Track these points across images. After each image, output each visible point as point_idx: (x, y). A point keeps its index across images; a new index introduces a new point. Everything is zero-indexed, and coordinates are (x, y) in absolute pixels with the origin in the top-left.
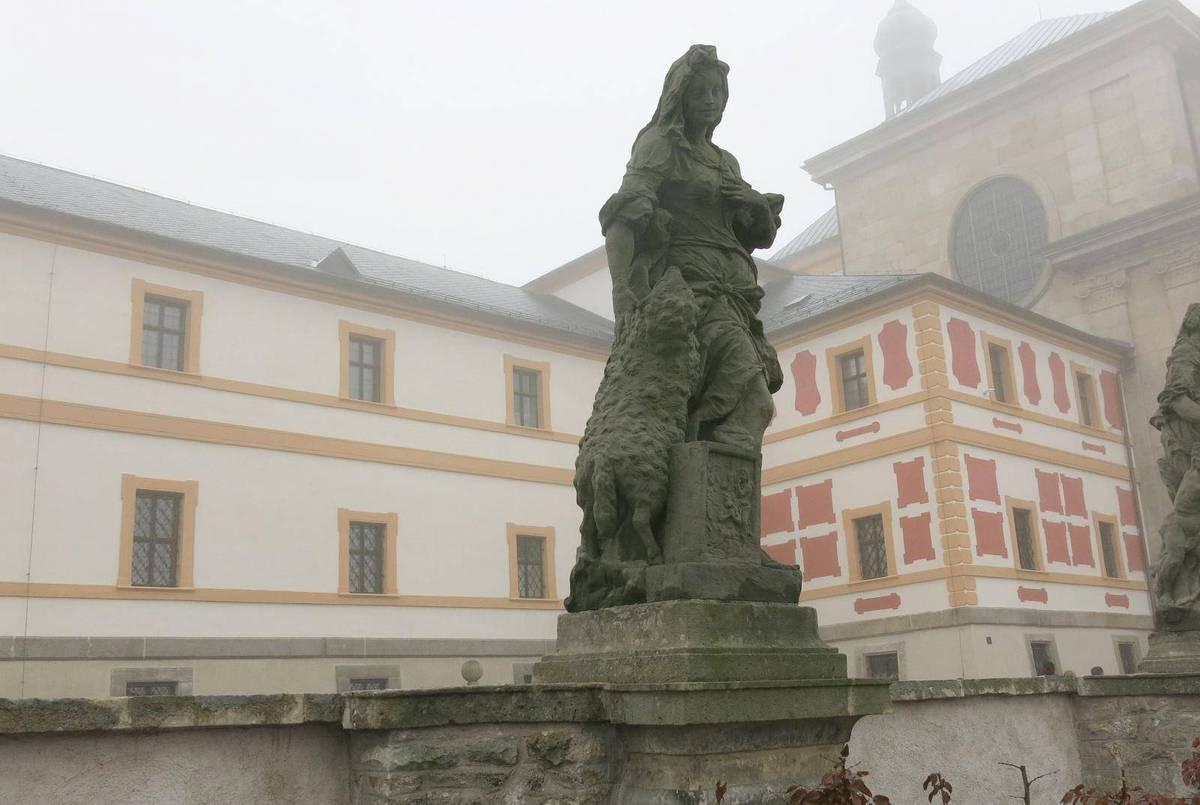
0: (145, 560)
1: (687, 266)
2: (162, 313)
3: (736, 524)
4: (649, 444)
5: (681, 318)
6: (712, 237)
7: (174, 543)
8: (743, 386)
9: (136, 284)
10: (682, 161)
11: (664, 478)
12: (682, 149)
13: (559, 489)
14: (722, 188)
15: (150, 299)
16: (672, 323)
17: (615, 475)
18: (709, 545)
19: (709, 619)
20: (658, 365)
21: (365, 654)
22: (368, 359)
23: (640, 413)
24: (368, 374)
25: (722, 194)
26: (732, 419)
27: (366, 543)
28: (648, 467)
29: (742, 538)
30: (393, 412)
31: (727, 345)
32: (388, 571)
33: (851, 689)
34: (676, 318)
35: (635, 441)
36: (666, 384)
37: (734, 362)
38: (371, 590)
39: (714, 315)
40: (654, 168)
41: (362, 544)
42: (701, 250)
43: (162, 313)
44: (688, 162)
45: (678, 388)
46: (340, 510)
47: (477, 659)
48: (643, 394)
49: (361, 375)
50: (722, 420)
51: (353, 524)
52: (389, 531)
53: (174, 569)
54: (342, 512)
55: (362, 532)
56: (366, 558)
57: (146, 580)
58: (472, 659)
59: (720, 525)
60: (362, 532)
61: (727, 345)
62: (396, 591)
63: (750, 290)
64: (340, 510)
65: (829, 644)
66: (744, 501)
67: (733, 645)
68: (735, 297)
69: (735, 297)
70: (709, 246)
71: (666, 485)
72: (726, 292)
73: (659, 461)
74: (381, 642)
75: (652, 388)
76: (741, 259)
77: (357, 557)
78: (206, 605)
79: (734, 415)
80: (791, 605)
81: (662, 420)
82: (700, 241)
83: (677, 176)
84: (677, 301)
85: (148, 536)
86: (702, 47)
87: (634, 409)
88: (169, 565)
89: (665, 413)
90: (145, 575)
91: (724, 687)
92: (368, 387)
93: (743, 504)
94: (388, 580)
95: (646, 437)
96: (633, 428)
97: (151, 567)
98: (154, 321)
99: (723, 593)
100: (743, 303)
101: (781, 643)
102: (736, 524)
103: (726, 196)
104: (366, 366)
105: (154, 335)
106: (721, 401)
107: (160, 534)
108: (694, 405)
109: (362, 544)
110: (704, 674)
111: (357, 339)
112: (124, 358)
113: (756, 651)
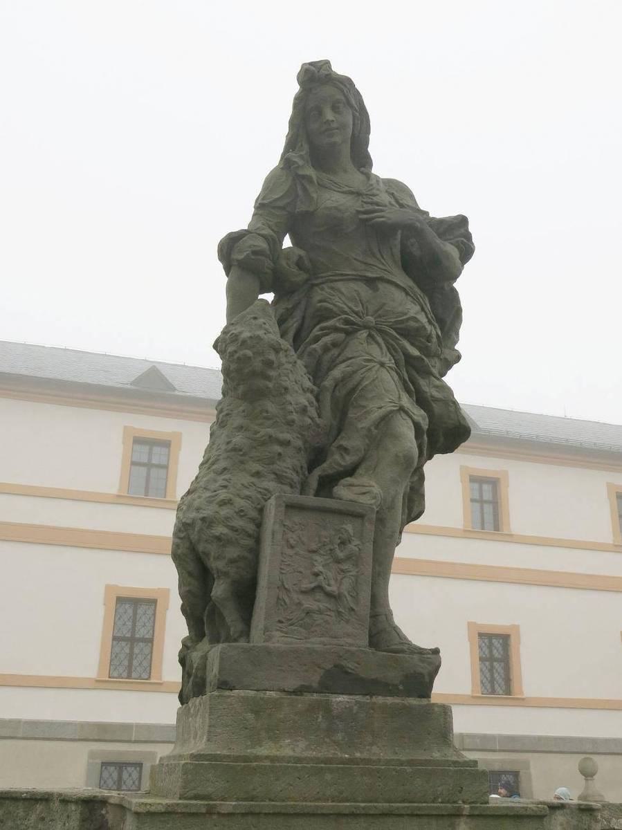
0: (488, 675)
1: (319, 305)
2: (150, 453)
3: (329, 595)
4: (223, 503)
5: (249, 353)
6: (355, 270)
7: (506, 661)
8: (369, 430)
9: (126, 429)
10: (305, 190)
11: (249, 542)
12: (304, 177)
13: (154, 558)
14: (358, 212)
15: (138, 441)
16: (239, 358)
17: (191, 543)
18: (280, 622)
19: (250, 716)
20: (244, 411)
21: (498, 748)
22: (487, 496)
23: (225, 469)
24: (488, 509)
25: (360, 219)
26: (360, 471)
27: (495, 651)
28: (220, 530)
29: (339, 613)
30: (511, 538)
31: (359, 384)
32: (514, 675)
33: (463, 820)
34: (241, 353)
35: (210, 501)
36: (256, 433)
37: (364, 403)
38: (501, 692)
39: (348, 353)
40: (271, 203)
41: (491, 652)
42: (339, 285)
43: (150, 453)
44: (311, 189)
45: (270, 437)
46: (469, 624)
47: (591, 756)
48: (230, 446)
49: (482, 509)
50: (351, 471)
51: (481, 635)
52: (513, 641)
53: (508, 680)
54: (471, 625)
55: (490, 642)
56: (495, 664)
57: (490, 690)
58: (588, 756)
59: (301, 597)
60: (490, 642)
61: (359, 384)
62: (522, 693)
63: (402, 322)
64: (469, 624)
65: (465, 753)
66: (345, 566)
67: (287, 752)
68: (380, 331)
69: (380, 331)
70: (349, 280)
71: (251, 550)
72: (365, 327)
73: (239, 523)
74: (512, 739)
75: (238, 439)
76: (393, 289)
77: (487, 663)
78: (608, 711)
79: (363, 466)
80: (413, 701)
81: (253, 476)
82: (342, 275)
83: (301, 207)
84: (241, 333)
85: (488, 656)
86: (311, 64)
87: (222, 464)
88: (489, 679)
89: (256, 467)
90: (489, 686)
91: (203, 810)
92: (489, 518)
93: (342, 571)
94: (515, 685)
95: (223, 495)
96: (213, 487)
97: (492, 681)
98: (477, 496)
99: (292, 683)
100: (395, 339)
101: (380, 752)
102: (329, 595)
103: (367, 220)
104: (486, 502)
105: (143, 471)
106: (346, 450)
107: (496, 654)
108: (317, 456)
109: (491, 652)
110: (210, 790)
111: (477, 480)
112: (114, 491)
113: (318, 760)
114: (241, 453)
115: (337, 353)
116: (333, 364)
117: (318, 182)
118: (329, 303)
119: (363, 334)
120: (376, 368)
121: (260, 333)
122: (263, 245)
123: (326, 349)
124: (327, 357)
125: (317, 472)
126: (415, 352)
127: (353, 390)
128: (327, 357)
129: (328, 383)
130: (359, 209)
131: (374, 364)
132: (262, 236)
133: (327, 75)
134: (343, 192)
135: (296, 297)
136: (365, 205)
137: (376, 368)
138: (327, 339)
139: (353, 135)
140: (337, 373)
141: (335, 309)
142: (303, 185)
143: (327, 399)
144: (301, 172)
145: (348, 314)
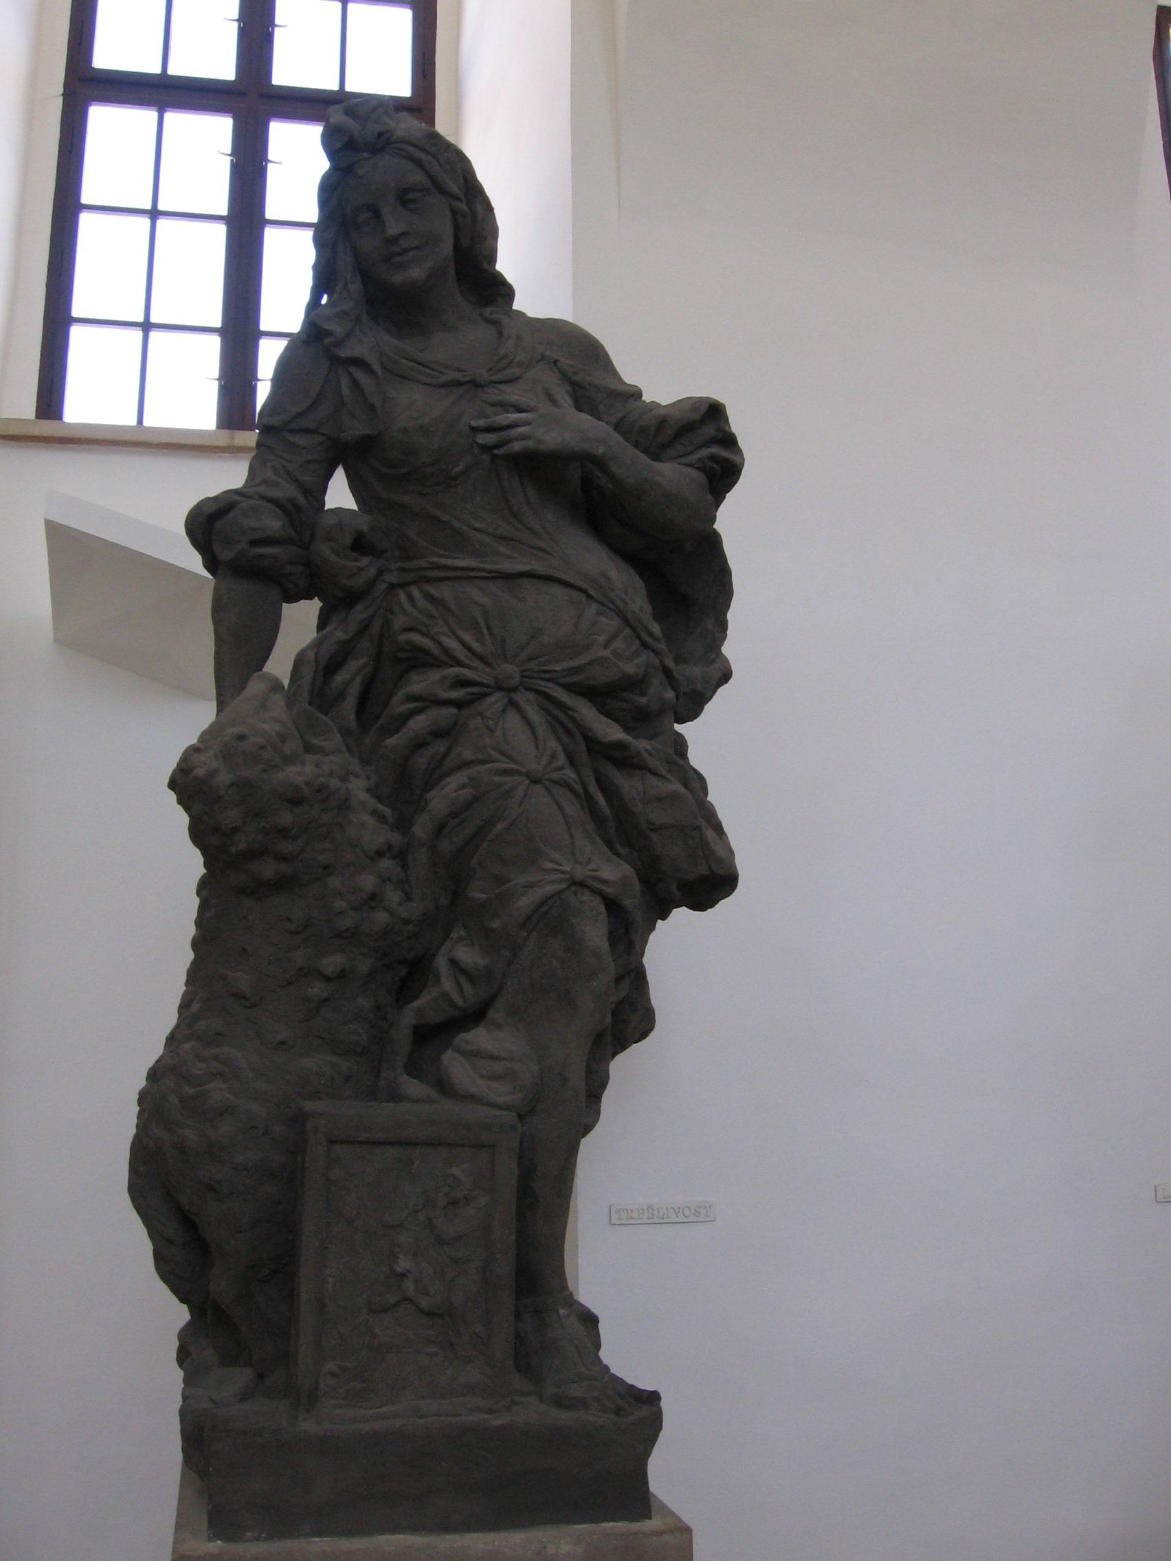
114: (247, 1004)
115: (442, 749)
116: (435, 777)
117: (383, 367)
118: (424, 634)
119: (495, 701)
120: (522, 789)
121: (252, 772)
122: (274, 524)
123: (419, 745)
124: (422, 760)
125: (407, 1018)
126: (612, 732)
127: (480, 834)
128: (422, 760)
129: (421, 828)
130: (474, 423)
131: (517, 778)
132: (274, 502)
133: (380, 135)
134: (443, 386)
135: (360, 613)
136: (489, 410)
137: (522, 789)
138: (419, 723)
139: (457, 246)
140: (440, 800)
141: (435, 650)
142: (350, 374)
143: (420, 858)
144: (345, 352)
145: (460, 664)
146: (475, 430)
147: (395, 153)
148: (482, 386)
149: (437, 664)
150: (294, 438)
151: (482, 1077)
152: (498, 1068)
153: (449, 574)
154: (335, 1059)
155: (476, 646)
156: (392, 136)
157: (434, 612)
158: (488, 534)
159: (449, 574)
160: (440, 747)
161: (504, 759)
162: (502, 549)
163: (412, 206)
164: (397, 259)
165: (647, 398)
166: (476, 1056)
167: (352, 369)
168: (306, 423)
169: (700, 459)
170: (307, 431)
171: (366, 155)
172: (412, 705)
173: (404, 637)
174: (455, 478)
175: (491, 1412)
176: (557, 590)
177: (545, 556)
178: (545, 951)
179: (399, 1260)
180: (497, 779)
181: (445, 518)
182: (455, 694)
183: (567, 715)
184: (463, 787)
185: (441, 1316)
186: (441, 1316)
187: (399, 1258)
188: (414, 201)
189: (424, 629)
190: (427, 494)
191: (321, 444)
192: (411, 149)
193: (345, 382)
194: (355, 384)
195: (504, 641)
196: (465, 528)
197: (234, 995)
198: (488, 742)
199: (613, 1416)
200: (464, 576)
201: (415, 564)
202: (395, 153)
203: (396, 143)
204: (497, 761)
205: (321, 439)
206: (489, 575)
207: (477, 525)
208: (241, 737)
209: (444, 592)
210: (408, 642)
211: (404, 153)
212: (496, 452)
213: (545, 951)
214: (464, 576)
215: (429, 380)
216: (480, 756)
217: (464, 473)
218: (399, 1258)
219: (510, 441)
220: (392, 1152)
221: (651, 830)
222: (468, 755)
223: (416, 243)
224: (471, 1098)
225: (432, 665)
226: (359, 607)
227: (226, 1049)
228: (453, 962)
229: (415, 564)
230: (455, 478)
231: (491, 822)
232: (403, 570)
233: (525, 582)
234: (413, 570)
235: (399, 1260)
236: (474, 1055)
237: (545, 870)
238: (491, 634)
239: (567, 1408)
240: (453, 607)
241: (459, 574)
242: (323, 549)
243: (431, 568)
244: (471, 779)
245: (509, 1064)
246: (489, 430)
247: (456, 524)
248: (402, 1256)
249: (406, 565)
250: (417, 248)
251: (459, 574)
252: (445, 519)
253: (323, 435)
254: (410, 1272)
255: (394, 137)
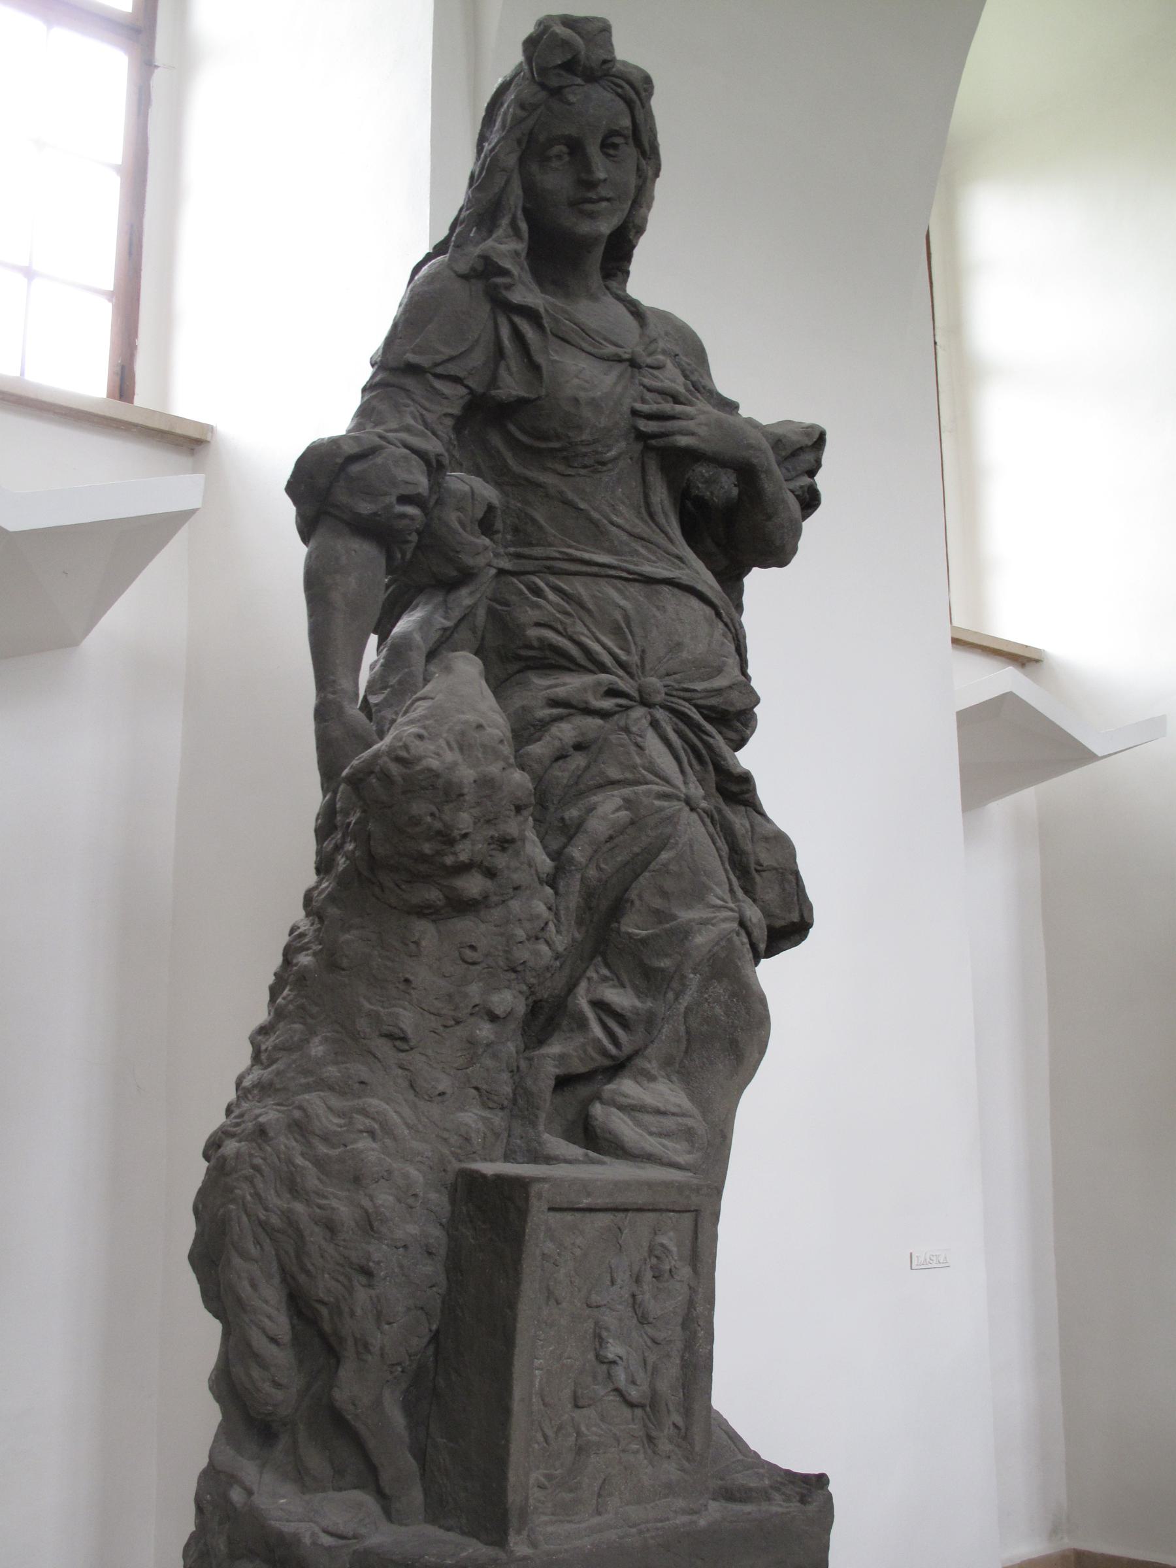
133: (605, 62)
134: (602, 358)
136: (649, 396)
141: (574, 651)
146: (635, 413)
147: (609, 86)
148: (640, 367)
149: (572, 666)
150: (438, 384)
151: (651, 1134)
152: (669, 1123)
153: (584, 568)
154: (486, 1114)
155: (623, 656)
156: (613, 67)
157: (568, 608)
158: (624, 530)
159: (584, 568)
160: (579, 760)
161: (658, 780)
162: (642, 551)
163: (612, 152)
164: (588, 207)
165: (744, 412)
166: (639, 1111)
167: (517, 320)
168: (452, 369)
169: (801, 487)
170: (456, 380)
171: (579, 81)
172: (555, 711)
173: (533, 633)
174: (603, 464)
175: (693, 1512)
176: (695, 603)
177: (682, 565)
178: (706, 996)
179: (609, 1345)
180: (657, 803)
181: (582, 505)
182: (608, 704)
183: (702, 740)
184: (618, 810)
185: (643, 1406)
186: (643, 1406)
187: (607, 1343)
188: (615, 146)
189: (560, 628)
190: (569, 475)
191: (462, 397)
192: (627, 87)
193: (505, 332)
194: (518, 335)
195: (643, 651)
196: (605, 522)
197: (390, 1036)
198: (638, 760)
199: (799, 1504)
200: (599, 572)
201: (538, 551)
202: (609, 86)
203: (614, 76)
204: (652, 783)
205: (464, 391)
206: (631, 577)
207: (615, 518)
208: (480, 727)
209: (578, 587)
210: (541, 640)
211: (619, 90)
212: (653, 442)
213: (706, 996)
214: (599, 572)
215: (593, 350)
216: (628, 775)
217: (615, 459)
218: (607, 1343)
219: (673, 434)
220: (604, 1219)
221: (757, 871)
222: (614, 773)
223: (611, 195)
224: (649, 1158)
225: (570, 670)
226: (464, 591)
227: (375, 1102)
228: (600, 1006)
229: (538, 551)
230: (603, 464)
231: (652, 852)
232: (518, 556)
233: (666, 589)
234: (536, 559)
235: (609, 1345)
236: (633, 1109)
237: (714, 906)
238: (635, 644)
239: (742, 1501)
240: (591, 607)
241: (595, 569)
242: (453, 517)
243: (564, 560)
244: (625, 800)
245: (680, 1120)
246: (650, 417)
247: (595, 515)
248: (611, 1341)
249: (526, 551)
250: (608, 200)
251: (595, 569)
252: (582, 507)
253: (467, 387)
254: (621, 1358)
255: (614, 69)
